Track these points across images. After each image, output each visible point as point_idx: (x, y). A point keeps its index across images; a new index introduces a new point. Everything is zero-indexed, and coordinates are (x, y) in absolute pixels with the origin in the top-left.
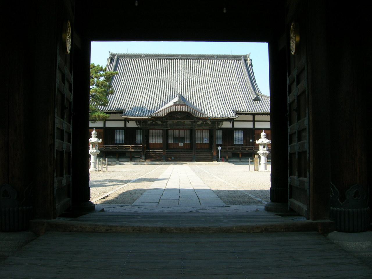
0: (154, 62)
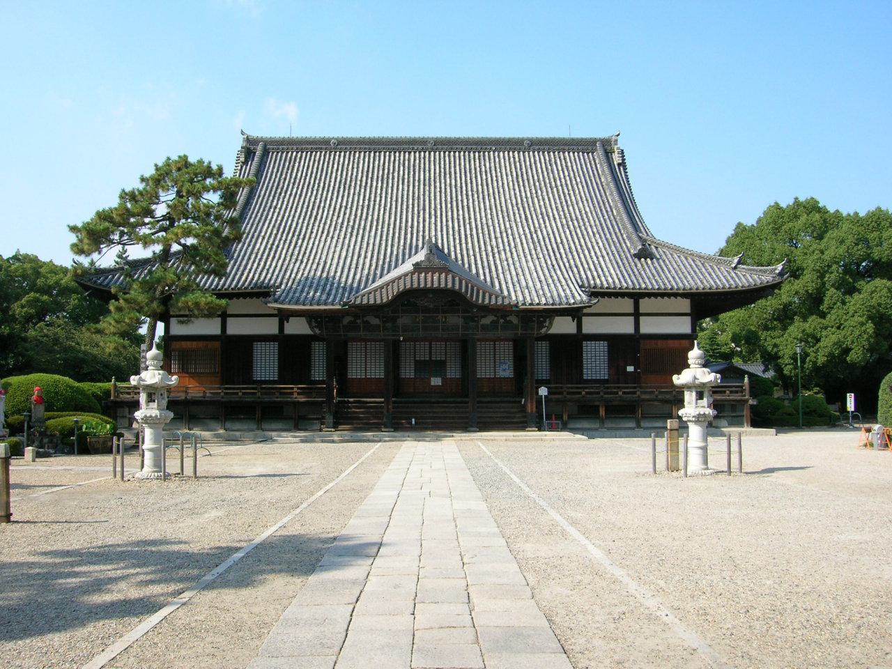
0: (363, 160)
